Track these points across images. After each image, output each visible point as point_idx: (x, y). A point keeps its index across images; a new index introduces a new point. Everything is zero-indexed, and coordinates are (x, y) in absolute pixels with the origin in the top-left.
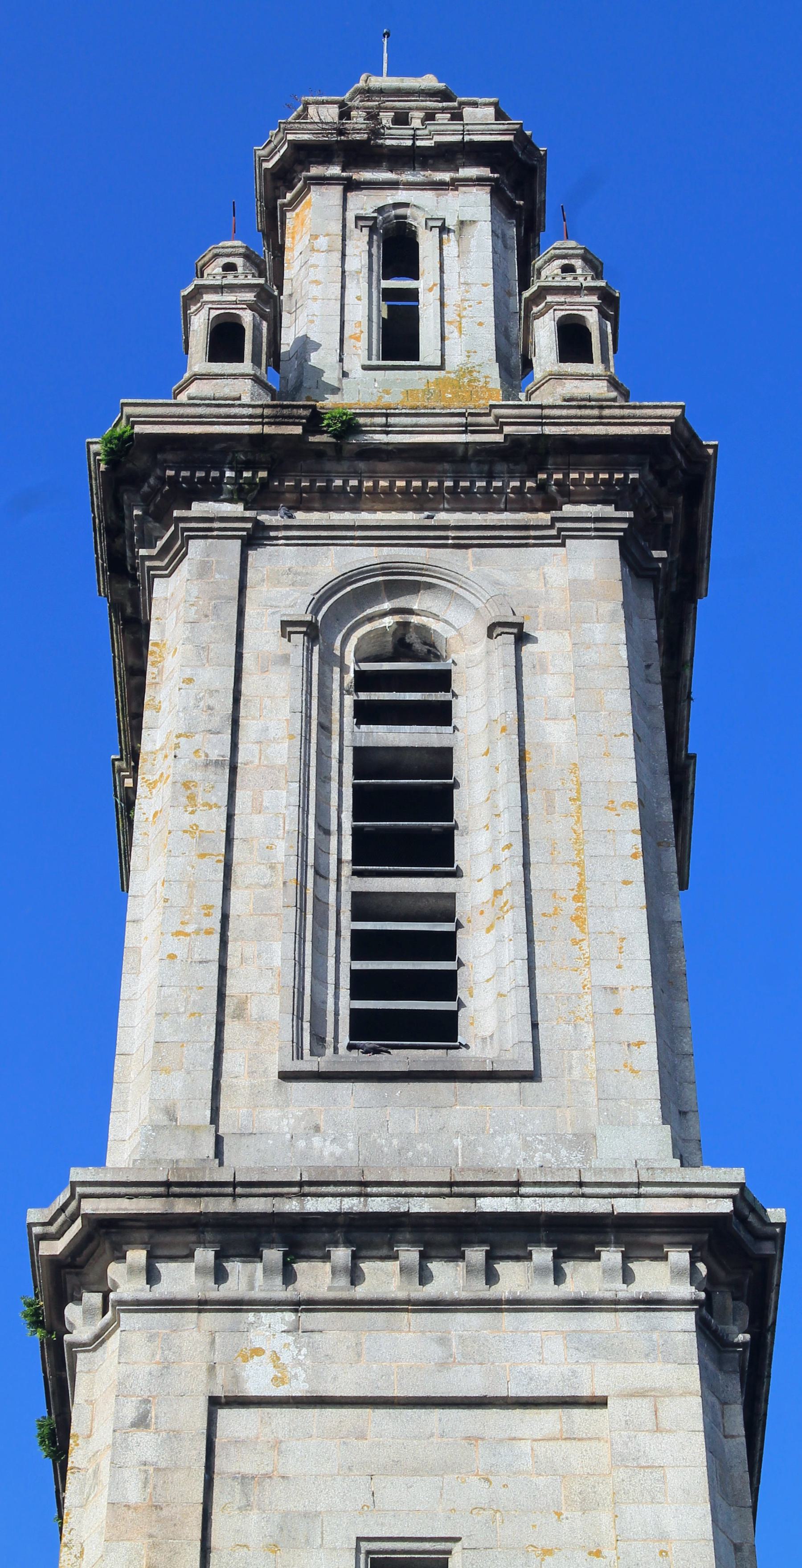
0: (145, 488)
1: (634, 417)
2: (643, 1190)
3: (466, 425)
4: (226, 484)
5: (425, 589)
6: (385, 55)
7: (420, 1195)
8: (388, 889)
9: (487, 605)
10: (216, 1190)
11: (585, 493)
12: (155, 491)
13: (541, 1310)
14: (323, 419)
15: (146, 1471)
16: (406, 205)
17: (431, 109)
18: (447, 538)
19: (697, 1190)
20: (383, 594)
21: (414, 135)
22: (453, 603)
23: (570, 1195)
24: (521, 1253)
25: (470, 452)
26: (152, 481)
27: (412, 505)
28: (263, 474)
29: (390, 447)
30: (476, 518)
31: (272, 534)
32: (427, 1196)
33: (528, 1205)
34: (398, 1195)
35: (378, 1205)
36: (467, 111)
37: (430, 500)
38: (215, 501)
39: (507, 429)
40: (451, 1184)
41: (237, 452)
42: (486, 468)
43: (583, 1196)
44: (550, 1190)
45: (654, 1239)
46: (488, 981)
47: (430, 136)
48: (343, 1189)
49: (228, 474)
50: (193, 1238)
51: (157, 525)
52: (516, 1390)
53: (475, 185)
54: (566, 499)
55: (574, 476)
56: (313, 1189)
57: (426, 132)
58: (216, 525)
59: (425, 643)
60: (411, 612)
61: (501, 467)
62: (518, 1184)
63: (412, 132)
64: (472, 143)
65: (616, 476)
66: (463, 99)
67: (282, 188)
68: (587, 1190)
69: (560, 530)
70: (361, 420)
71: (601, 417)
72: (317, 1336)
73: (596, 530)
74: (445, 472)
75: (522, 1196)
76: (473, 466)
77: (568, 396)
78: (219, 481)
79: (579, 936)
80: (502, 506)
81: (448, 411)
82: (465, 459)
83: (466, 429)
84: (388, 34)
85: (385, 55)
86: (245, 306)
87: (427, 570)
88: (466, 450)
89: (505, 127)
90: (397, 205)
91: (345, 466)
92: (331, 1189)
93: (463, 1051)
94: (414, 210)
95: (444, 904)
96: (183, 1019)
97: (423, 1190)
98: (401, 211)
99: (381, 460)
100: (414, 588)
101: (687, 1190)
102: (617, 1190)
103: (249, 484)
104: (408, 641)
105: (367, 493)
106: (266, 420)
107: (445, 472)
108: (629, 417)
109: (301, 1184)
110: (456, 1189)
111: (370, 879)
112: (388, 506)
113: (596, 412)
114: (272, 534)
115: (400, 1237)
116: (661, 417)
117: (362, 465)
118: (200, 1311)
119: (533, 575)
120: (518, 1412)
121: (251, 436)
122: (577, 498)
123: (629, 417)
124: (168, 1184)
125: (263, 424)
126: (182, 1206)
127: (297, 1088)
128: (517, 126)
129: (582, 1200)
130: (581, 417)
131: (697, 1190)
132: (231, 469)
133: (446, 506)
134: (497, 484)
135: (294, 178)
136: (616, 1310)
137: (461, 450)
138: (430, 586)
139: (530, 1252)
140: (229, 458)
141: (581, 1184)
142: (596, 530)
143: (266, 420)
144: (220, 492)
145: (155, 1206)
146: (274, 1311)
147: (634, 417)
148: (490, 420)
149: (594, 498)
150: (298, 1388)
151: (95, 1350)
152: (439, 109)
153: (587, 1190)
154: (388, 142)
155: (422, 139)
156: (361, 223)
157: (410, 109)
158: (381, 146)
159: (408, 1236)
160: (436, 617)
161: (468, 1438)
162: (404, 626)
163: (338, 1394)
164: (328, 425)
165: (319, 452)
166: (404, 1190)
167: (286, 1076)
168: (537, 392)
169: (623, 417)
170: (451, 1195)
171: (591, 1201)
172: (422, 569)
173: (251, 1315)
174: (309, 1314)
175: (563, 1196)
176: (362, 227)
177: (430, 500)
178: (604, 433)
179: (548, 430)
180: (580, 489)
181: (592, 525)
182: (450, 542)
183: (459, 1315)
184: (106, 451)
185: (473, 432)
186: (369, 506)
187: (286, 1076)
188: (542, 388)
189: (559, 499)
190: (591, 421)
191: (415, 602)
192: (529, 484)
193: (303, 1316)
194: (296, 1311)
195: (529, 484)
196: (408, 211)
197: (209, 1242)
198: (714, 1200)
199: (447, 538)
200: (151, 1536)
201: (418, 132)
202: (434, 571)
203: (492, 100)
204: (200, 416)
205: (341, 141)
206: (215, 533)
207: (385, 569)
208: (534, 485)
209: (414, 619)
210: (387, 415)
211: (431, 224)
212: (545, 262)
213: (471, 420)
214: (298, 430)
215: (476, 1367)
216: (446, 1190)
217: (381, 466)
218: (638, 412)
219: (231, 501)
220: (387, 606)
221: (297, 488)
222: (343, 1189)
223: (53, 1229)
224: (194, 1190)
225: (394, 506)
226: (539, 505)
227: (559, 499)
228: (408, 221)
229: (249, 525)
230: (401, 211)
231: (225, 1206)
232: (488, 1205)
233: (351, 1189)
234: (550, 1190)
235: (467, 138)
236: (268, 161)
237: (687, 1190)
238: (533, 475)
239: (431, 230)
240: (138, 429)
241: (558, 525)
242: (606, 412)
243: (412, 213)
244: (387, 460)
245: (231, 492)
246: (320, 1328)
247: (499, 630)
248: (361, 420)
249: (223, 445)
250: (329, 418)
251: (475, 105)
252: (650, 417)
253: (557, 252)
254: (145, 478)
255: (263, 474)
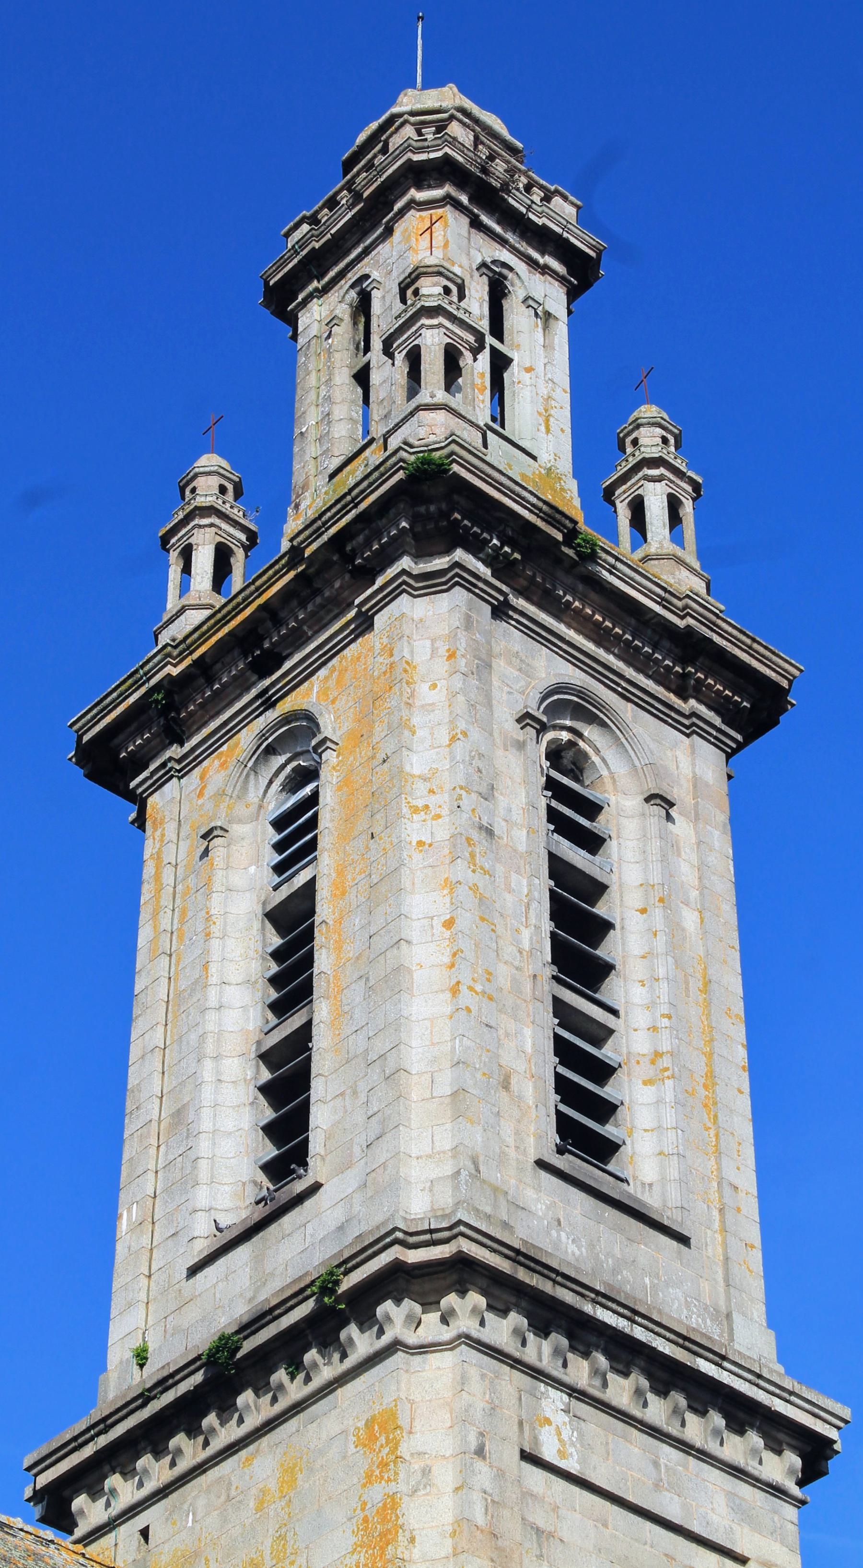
0: (422, 509)
1: (770, 660)
2: (793, 1398)
3: (663, 599)
4: (490, 547)
5: (598, 724)
6: (420, 42)
7: (664, 1337)
8: (574, 1004)
9: (645, 768)
10: (546, 1272)
11: (710, 698)
12: (428, 517)
13: (712, 1465)
14: (576, 538)
15: (486, 1500)
16: (511, 269)
17: (533, 180)
18: (618, 685)
19: (822, 1414)
20: (569, 711)
21: (530, 206)
22: (614, 747)
23: (750, 1381)
24: (700, 1408)
25: (655, 620)
26: (432, 508)
27: (595, 637)
28: (517, 556)
29: (608, 586)
30: (630, 672)
31: (511, 613)
32: (668, 1340)
33: (725, 1378)
34: (652, 1331)
35: (639, 1333)
36: (557, 200)
37: (610, 641)
38: (473, 555)
39: (690, 621)
40: (685, 1338)
41: (508, 526)
42: (656, 638)
43: (757, 1385)
44: (740, 1372)
45: (781, 1436)
46: (646, 1130)
47: (540, 215)
48: (621, 1310)
49: (495, 541)
50: (513, 1300)
51: (413, 542)
52: (696, 1527)
53: (557, 280)
54: (694, 694)
55: (710, 681)
56: (604, 1301)
57: (539, 209)
58: (481, 585)
59: (574, 763)
60: (580, 735)
61: (666, 643)
62: (724, 1358)
63: (529, 202)
64: (567, 240)
65: (736, 698)
66: (560, 188)
67: (410, 181)
68: (762, 1383)
69: (694, 724)
70: (603, 555)
71: (750, 647)
72: (582, 1422)
73: (716, 738)
74: (629, 625)
75: (723, 1368)
76: (649, 632)
77: (695, 591)
78: (487, 542)
79: (709, 1125)
80: (650, 673)
81: (656, 580)
82: (646, 623)
83: (662, 602)
84: (422, 18)
85: (420, 42)
86: (468, 347)
87: (607, 710)
88: (654, 617)
89: (594, 243)
90: (504, 265)
91: (569, 580)
92: (614, 1306)
93: (625, 1184)
94: (515, 277)
95: (602, 1034)
96: (479, 1075)
97: (668, 1335)
98: (505, 272)
99: (594, 590)
100: (592, 719)
101: (816, 1411)
102: (777, 1391)
103: (504, 557)
104: (563, 754)
105: (613, 636)
106: (541, 514)
107: (629, 625)
108: (767, 659)
109: (598, 1293)
110: (687, 1344)
111: (563, 989)
112: (581, 628)
113: (748, 641)
114: (511, 613)
115: (637, 1361)
116: (785, 671)
117: (580, 587)
118: (512, 1367)
119: (669, 753)
120: (694, 1546)
121: (528, 522)
122: (701, 698)
123: (767, 659)
124: (518, 1252)
125: (538, 516)
126: (522, 1275)
127: (544, 1175)
128: (602, 248)
129: (755, 1388)
130: (738, 640)
131: (822, 1414)
132: (498, 539)
133: (616, 651)
134: (657, 656)
135: (425, 180)
136: (754, 1486)
137: (651, 615)
138: (603, 724)
139: (708, 1411)
140: (501, 528)
141: (759, 1376)
142: (716, 738)
143: (541, 514)
144: (481, 550)
145: (504, 1265)
146: (557, 1389)
147: (770, 660)
148: (680, 604)
149: (712, 704)
150: (572, 1466)
151: (412, 1354)
152: (539, 184)
153: (762, 1383)
154: (511, 200)
155: (534, 213)
156: (484, 270)
157: (499, 155)
158: (505, 200)
159: (642, 1364)
160: (597, 751)
161: (666, 1555)
162: (571, 744)
163: (597, 1483)
164: (579, 545)
165: (560, 560)
166: (657, 1329)
167: (541, 1164)
168: (656, 562)
169: (763, 656)
170: (682, 1346)
171: (761, 1392)
172: (604, 707)
173: (542, 1385)
174: (577, 1402)
175: (745, 1379)
176: (484, 274)
177: (610, 641)
178: (748, 662)
179: (716, 639)
180: (708, 692)
181: (714, 733)
182: (620, 689)
183: (664, 1445)
184: (418, 467)
185: (665, 607)
186: (567, 620)
187: (541, 1164)
188: (662, 561)
189: (691, 691)
190: (743, 647)
191: (588, 731)
192: (677, 669)
193: (573, 1401)
194: (570, 1395)
195: (677, 669)
196: (510, 275)
197: (522, 1308)
198: (828, 1426)
199: (618, 685)
200: (492, 1561)
201: (534, 206)
202: (612, 714)
203: (579, 203)
204: (501, 484)
205: (481, 179)
206: (477, 591)
207: (580, 693)
208: (681, 671)
209: (581, 743)
210: (617, 559)
211: (531, 302)
212: (648, 424)
213: (667, 596)
214: (559, 537)
215: (676, 1497)
216: (681, 1341)
217: (593, 596)
218: (774, 658)
219: (484, 562)
220: (568, 723)
221: (532, 580)
222: (621, 1310)
223: (412, 1240)
224: (532, 1265)
225: (584, 630)
226: (673, 687)
227: (691, 691)
228: (506, 283)
229: (502, 598)
230: (505, 272)
231: (547, 1287)
232: (705, 1367)
233: (626, 1312)
234: (740, 1372)
235: (565, 235)
236: (414, 153)
237: (816, 1411)
238: (684, 662)
239: (481, 276)
240: (455, 468)
241: (694, 720)
242: (755, 646)
243: (512, 278)
244: (597, 593)
245: (488, 555)
246: (583, 1417)
247: (658, 801)
248: (603, 555)
249: (503, 516)
250: (582, 539)
251: (565, 198)
252: (779, 667)
253: (663, 422)
254: (428, 501)
255: (517, 556)
